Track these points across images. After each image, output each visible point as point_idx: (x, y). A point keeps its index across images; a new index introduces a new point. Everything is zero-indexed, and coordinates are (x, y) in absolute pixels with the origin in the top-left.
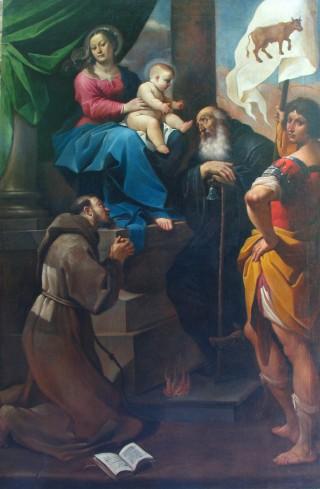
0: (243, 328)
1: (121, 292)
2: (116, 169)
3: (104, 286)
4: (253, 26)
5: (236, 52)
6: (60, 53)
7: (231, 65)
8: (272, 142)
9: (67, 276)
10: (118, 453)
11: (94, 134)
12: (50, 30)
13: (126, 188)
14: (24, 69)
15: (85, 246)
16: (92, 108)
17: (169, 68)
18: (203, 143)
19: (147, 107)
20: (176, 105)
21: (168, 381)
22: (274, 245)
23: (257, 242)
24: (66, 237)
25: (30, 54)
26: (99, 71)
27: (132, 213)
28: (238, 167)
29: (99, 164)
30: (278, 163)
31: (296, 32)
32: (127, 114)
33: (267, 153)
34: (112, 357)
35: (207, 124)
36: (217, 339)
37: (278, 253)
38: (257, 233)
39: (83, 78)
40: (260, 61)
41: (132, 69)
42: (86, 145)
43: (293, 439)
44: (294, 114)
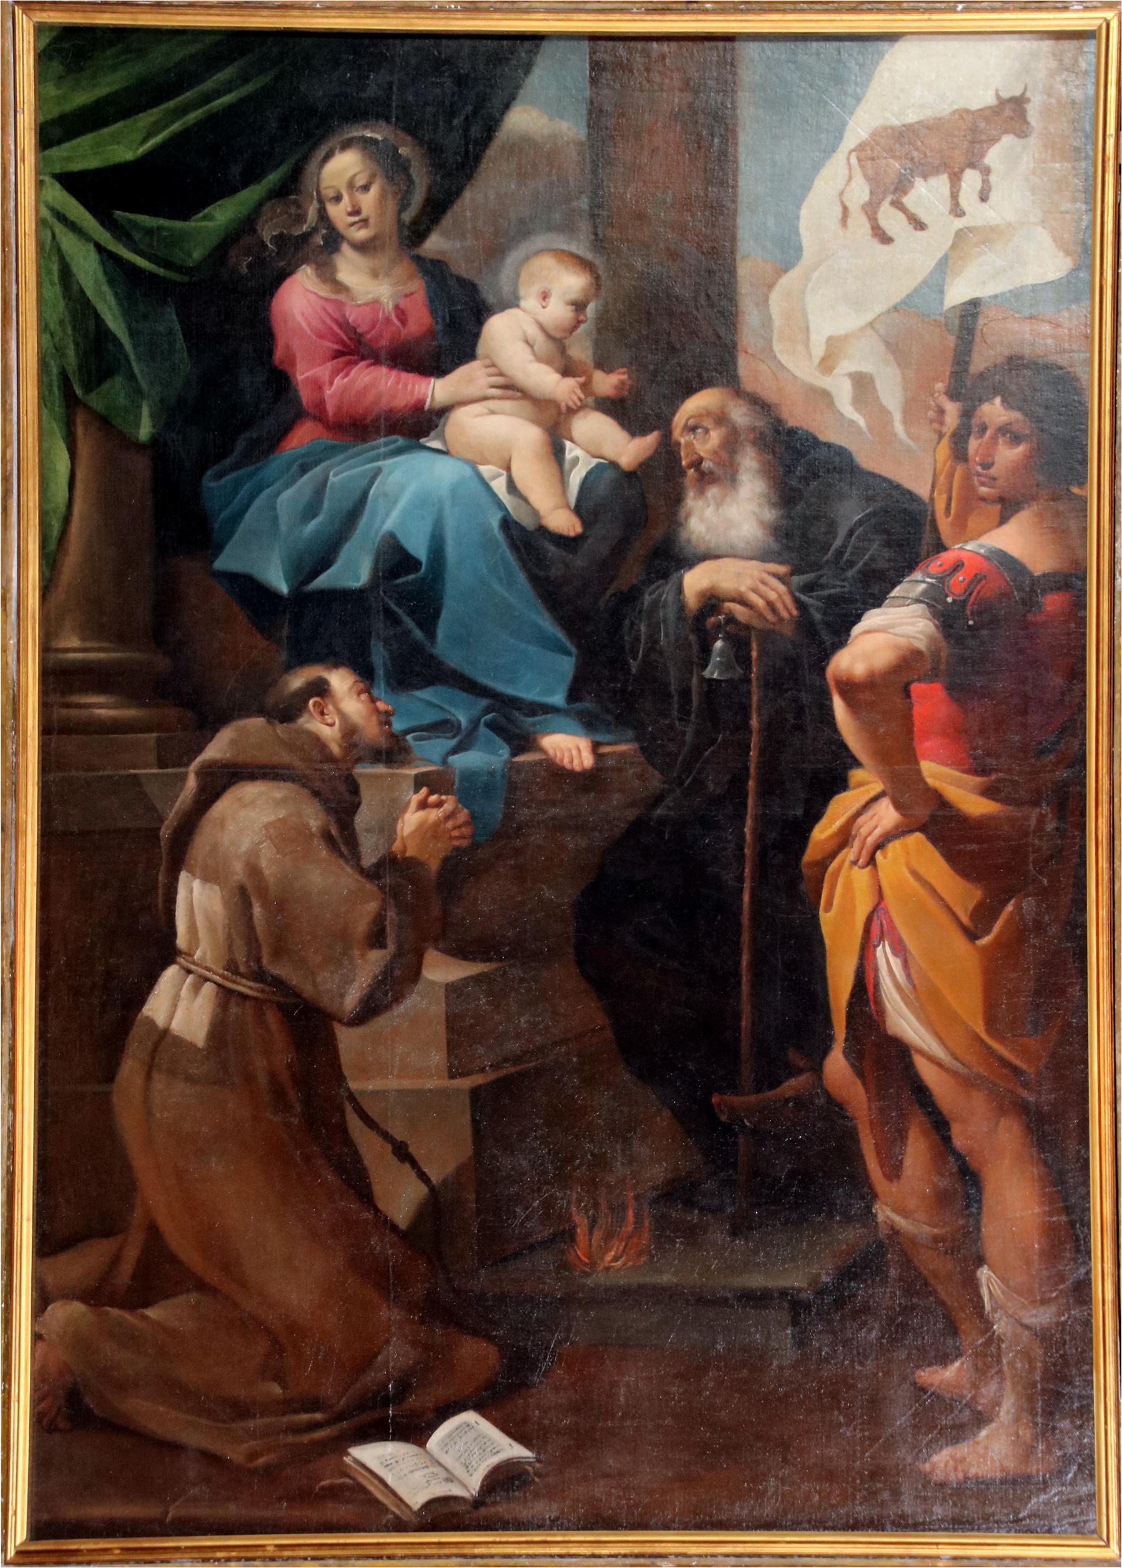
0: (817, 1069)
1: (432, 956)
2: (410, 582)
3: (376, 938)
4: (860, 127)
5: (804, 212)
6: (222, 215)
7: (788, 252)
8: (911, 496)
9: (257, 910)
10: (421, 1442)
11: (342, 474)
12: (184, 135)
13: (445, 646)
14: (103, 263)
15: (314, 818)
16: (328, 392)
17: (585, 264)
18: (691, 501)
19: (511, 389)
20: (606, 383)
21: (581, 1222)
22: (922, 813)
23: (863, 805)
24: (250, 790)
25: (118, 214)
26: (351, 269)
27: (463, 718)
28: (810, 577)
29: (354, 569)
30: (938, 564)
31: (1007, 140)
32: (444, 411)
33: (904, 533)
34: (402, 1152)
35: (707, 444)
36: (736, 1100)
37: (934, 840)
38: (866, 780)
39: (300, 299)
40: (885, 239)
41: (461, 268)
42: (311, 510)
43: (982, 1404)
44: (994, 411)
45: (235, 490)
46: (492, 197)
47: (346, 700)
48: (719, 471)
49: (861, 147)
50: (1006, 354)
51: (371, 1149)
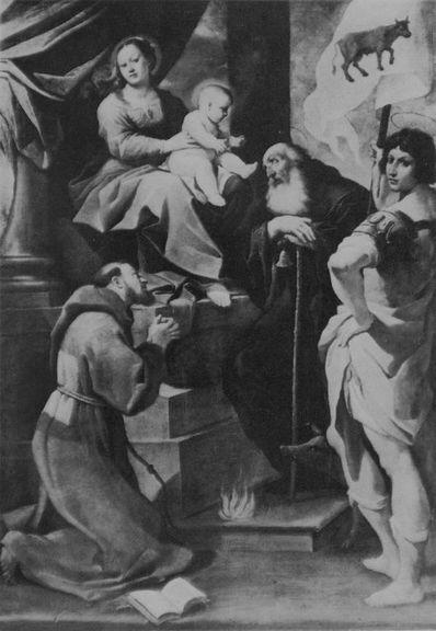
3: (140, 378)
6: (78, 72)
11: (127, 181)
12: (65, 40)
15: (116, 328)
20: (236, 141)
25: (36, 74)
29: (131, 221)
30: (375, 217)
32: (169, 154)
33: (359, 204)
34: (151, 469)
35: (277, 168)
38: (344, 310)
39: (110, 112)
40: (351, 80)
42: (114, 196)
44: (397, 153)
45: (82, 189)
46: (192, 425)
47: (127, 279)
48: (283, 179)
49: (339, 43)
50: (411, 584)
51: (138, 466)
